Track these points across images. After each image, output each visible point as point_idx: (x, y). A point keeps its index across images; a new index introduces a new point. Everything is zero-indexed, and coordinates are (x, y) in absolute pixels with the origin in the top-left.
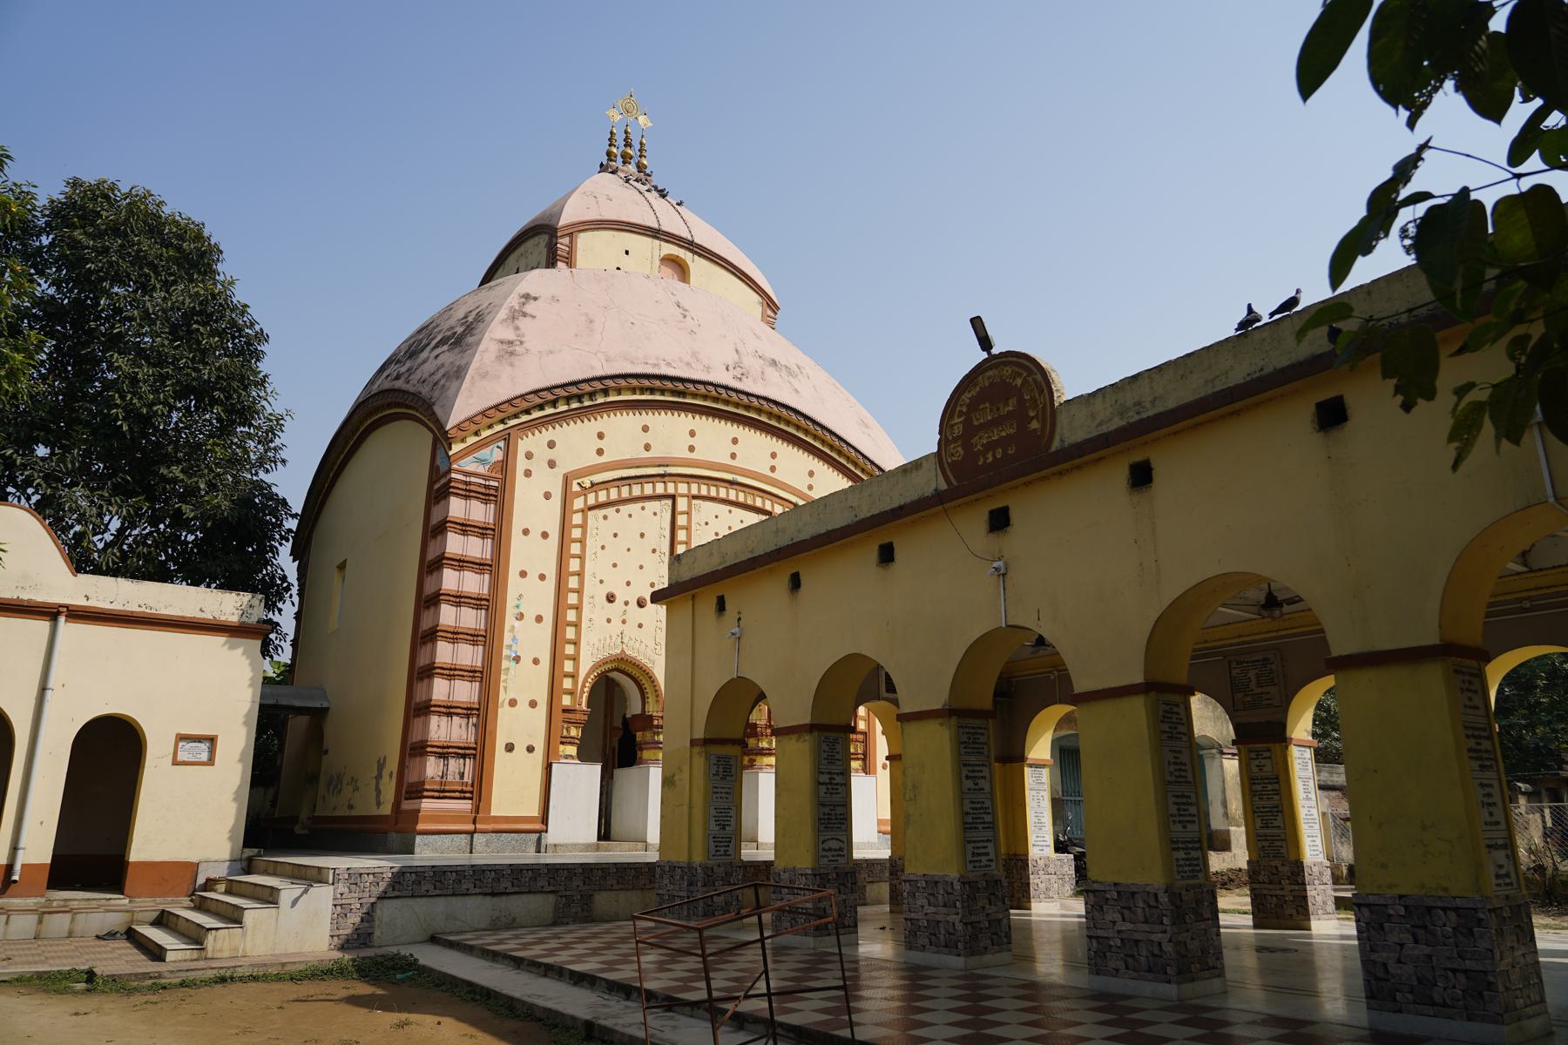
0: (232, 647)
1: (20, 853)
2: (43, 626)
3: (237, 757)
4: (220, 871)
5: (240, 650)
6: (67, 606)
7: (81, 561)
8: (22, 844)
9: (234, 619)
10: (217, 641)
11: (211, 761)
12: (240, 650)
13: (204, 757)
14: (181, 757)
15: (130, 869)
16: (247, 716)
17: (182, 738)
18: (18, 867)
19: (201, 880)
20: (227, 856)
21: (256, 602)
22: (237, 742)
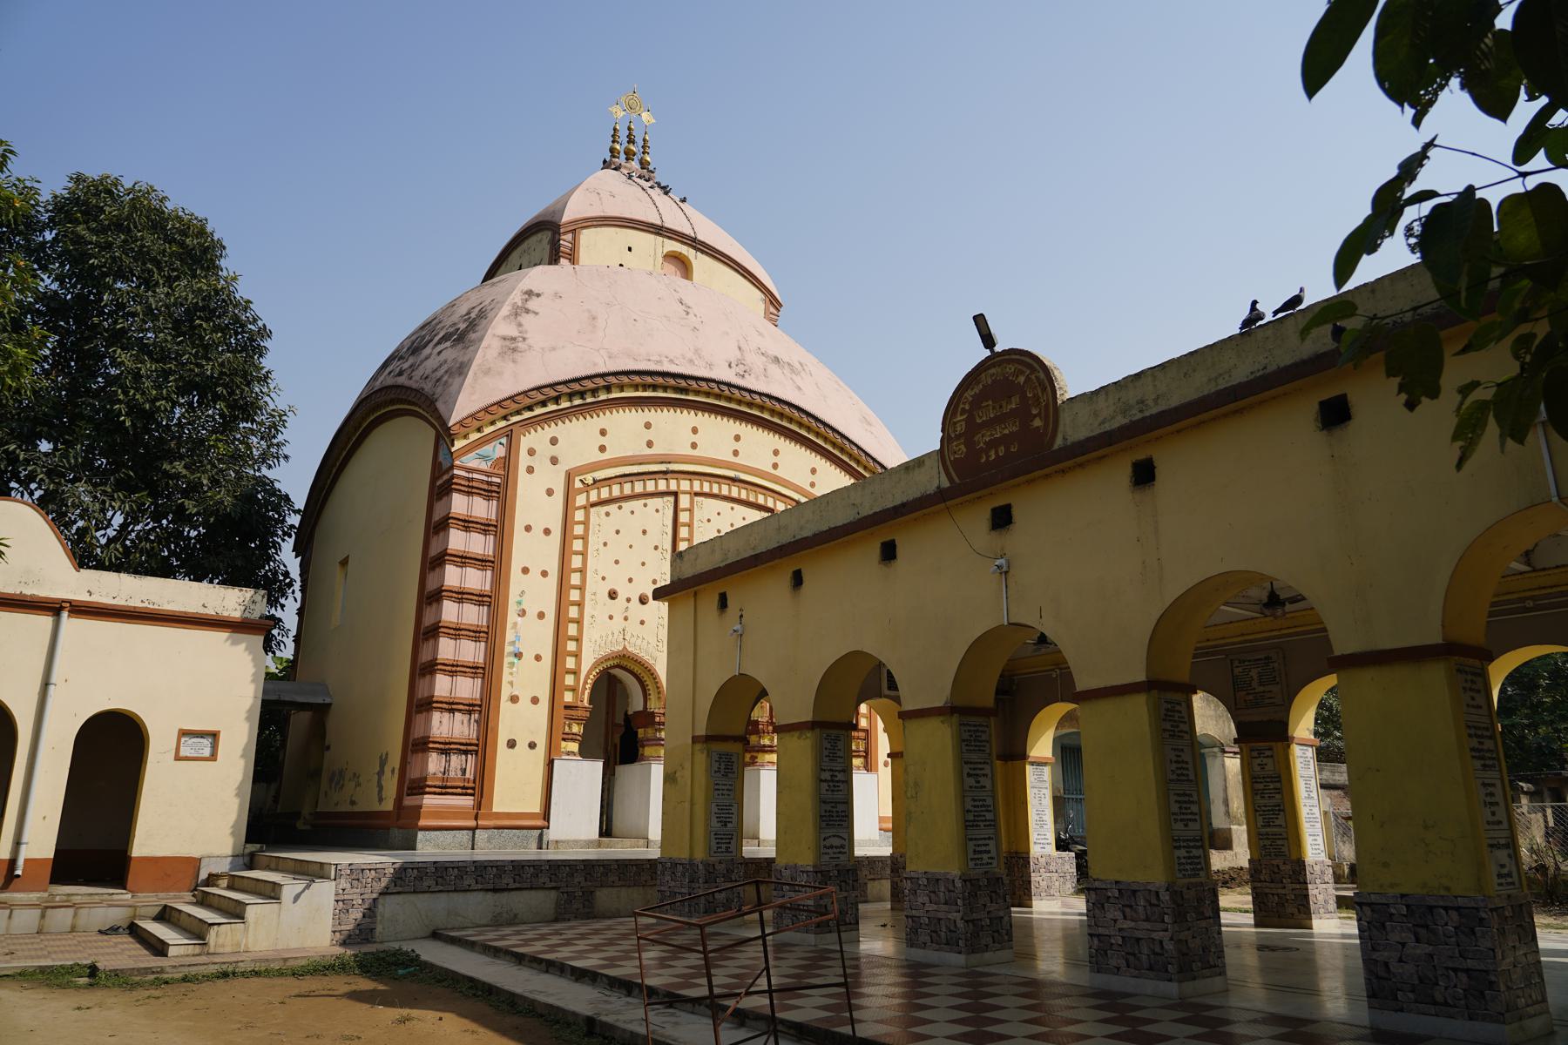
0: (234, 643)
1: (23, 847)
2: (46, 621)
3: (240, 752)
4: (223, 867)
5: (243, 646)
6: (70, 602)
7: (84, 557)
8: (25, 839)
9: (236, 614)
10: (221, 636)
11: (213, 757)
12: (243, 646)
13: (207, 752)
14: (184, 752)
15: (133, 864)
16: (239, 788)
17: (184, 733)
18: (21, 862)
19: (203, 875)
20: (229, 852)
21: (258, 598)
22: (239, 737)
